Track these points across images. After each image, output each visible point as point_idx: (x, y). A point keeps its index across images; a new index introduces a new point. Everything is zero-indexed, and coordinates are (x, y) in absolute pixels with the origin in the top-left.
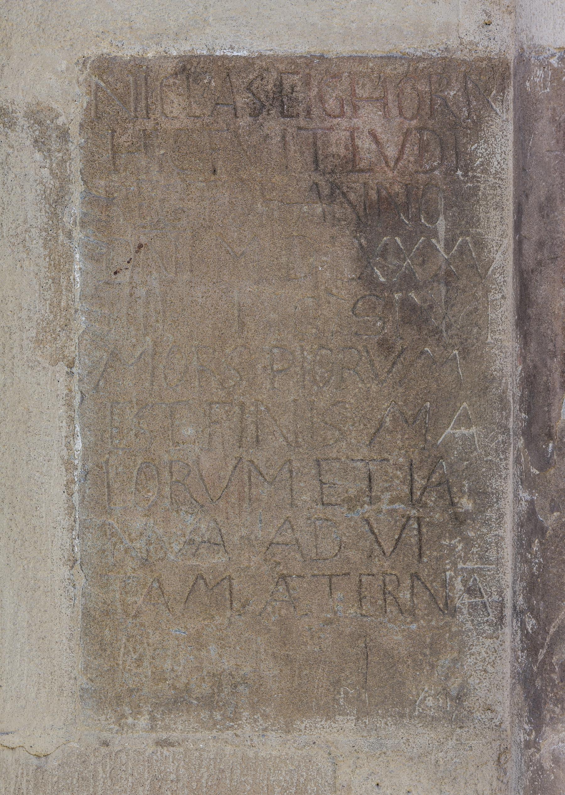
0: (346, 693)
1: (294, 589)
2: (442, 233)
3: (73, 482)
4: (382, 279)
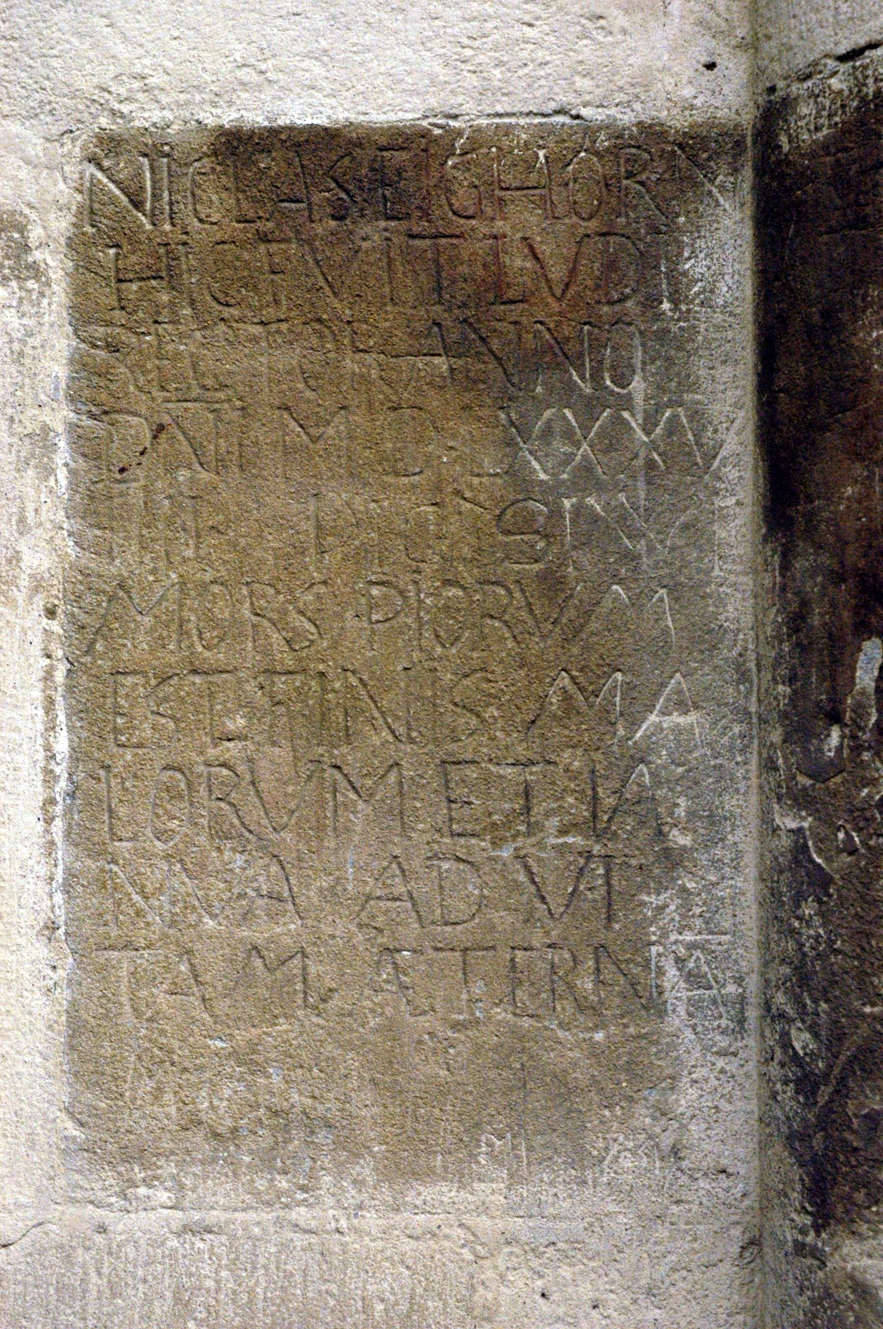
0: (490, 1145)
1: (208, 216)
2: (639, 400)
3: (52, 801)
4: (543, 476)
